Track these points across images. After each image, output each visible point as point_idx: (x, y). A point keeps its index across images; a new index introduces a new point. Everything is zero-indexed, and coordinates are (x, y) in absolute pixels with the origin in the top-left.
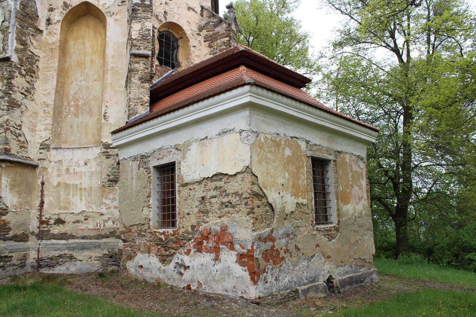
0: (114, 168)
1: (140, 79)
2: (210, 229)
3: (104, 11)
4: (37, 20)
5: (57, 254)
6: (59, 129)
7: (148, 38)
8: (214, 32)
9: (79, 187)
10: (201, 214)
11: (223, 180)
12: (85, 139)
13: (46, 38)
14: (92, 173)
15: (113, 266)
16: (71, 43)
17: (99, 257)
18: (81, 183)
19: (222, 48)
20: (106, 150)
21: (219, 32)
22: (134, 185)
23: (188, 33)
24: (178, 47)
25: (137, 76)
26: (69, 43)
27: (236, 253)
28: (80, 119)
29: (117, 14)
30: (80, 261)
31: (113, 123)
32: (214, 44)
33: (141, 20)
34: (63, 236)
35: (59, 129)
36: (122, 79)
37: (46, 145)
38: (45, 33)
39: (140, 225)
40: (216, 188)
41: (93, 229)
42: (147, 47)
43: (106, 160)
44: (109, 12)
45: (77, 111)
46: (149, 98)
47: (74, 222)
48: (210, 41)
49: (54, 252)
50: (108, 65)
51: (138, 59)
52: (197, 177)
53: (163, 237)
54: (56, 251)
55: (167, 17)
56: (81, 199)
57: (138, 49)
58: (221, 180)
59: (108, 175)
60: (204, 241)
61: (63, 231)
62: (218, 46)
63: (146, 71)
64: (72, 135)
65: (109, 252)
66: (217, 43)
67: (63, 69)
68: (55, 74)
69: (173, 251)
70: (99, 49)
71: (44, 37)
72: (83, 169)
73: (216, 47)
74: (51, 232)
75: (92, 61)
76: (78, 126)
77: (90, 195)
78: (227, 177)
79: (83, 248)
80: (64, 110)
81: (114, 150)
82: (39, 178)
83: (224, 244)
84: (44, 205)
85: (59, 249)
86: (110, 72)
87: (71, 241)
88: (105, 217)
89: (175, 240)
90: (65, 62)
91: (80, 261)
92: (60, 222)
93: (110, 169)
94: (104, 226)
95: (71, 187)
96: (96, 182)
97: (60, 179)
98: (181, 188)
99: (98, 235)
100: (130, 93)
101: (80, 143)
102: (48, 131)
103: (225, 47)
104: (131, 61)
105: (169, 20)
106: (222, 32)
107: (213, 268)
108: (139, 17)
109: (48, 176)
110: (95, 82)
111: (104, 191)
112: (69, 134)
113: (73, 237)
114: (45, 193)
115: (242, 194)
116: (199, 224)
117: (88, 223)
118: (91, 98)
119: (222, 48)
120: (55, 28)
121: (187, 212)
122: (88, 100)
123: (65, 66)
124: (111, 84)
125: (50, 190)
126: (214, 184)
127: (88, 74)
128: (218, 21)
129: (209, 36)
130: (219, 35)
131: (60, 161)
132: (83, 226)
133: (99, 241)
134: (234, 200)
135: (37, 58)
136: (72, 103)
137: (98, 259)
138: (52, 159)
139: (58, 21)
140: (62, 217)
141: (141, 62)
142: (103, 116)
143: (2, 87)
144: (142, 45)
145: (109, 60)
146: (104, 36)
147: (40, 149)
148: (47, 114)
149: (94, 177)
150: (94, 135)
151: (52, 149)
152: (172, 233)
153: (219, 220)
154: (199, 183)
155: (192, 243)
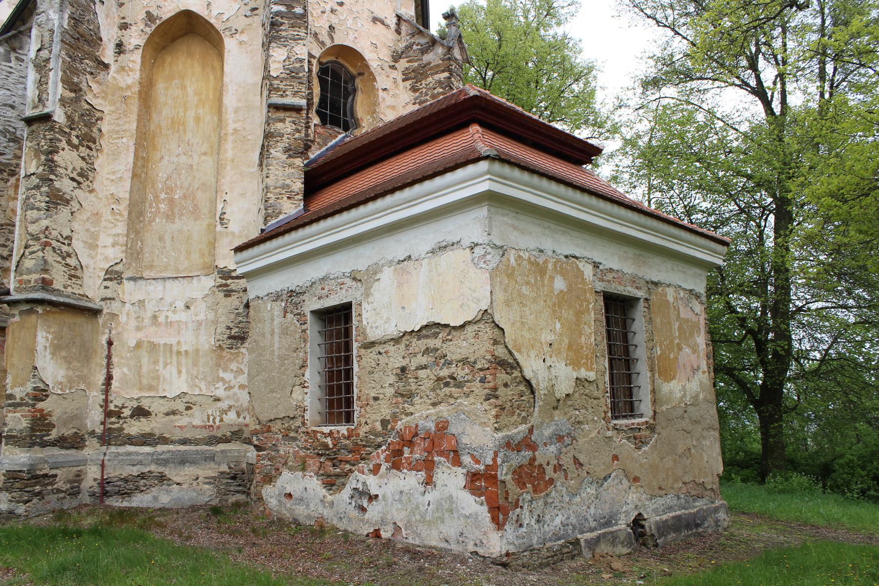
0: (238, 314)
1: (286, 150)
2: (417, 426)
3: (219, 26)
4: (99, 45)
5: (135, 471)
6: (139, 243)
7: (301, 75)
8: (421, 62)
9: (175, 349)
10: (400, 399)
11: (440, 336)
12: (186, 262)
13: (114, 78)
14: (200, 324)
15: (237, 495)
16: (160, 86)
17: (213, 478)
18: (179, 342)
19: (436, 91)
20: (224, 282)
21: (429, 63)
22: (276, 345)
23: (374, 64)
24: (355, 91)
25: (281, 146)
26: (157, 87)
27: (465, 471)
28: (178, 225)
29: (242, 32)
30: (178, 484)
31: (237, 232)
32: (421, 85)
33: (286, 43)
34: (146, 439)
35: (139, 243)
36: (252, 150)
37: (116, 272)
38: (113, 68)
39: (288, 419)
40: (427, 351)
41: (201, 427)
42: (297, 92)
43: (224, 299)
44: (229, 29)
45: (172, 211)
46: (303, 186)
47: (167, 414)
48: (413, 79)
49: (131, 467)
50: (227, 125)
51: (281, 115)
52: (392, 330)
53: (329, 441)
54: (134, 465)
55: (334, 36)
56: (179, 372)
57: (282, 96)
58: (436, 335)
59: (229, 328)
60: (405, 448)
61: (147, 430)
62: (428, 89)
63: (297, 135)
64: (162, 254)
65: (230, 468)
66: (428, 83)
67: (145, 134)
68: (132, 143)
69: (348, 467)
70: (211, 96)
71: (112, 76)
72: (183, 316)
73: (424, 90)
74: (125, 432)
75: (198, 119)
76: (173, 237)
77: (195, 365)
78: (447, 330)
79: (183, 461)
80: (147, 209)
81: (239, 281)
82: (104, 333)
83: (441, 453)
84: (113, 382)
85: (140, 463)
86: (231, 138)
87: (161, 448)
88: (223, 405)
89: (351, 446)
90: (149, 121)
91: (178, 484)
92: (140, 412)
93: (233, 316)
94: (221, 420)
95: (162, 349)
96: (207, 341)
97: (140, 335)
98: (363, 351)
99: (211, 437)
100: (267, 177)
101: (177, 270)
102: (120, 247)
103: (441, 90)
104: (269, 117)
105: (337, 42)
106: (436, 63)
107: (421, 498)
108: (283, 37)
109: (120, 329)
110: (203, 158)
111: (221, 357)
112: (157, 253)
113: (164, 440)
114: (115, 359)
115: (475, 362)
116: (395, 417)
117: (192, 416)
118: (196, 186)
119: (436, 91)
120: (132, 59)
121: (373, 395)
122: (191, 189)
123: (149, 129)
124: (233, 160)
125: (124, 355)
126: (422, 344)
127: (191, 143)
128: (427, 43)
129: (413, 71)
130: (431, 69)
131: (141, 302)
132: (183, 421)
133: (211, 448)
134: (462, 373)
135: (98, 114)
136: (163, 196)
137: (211, 480)
138: (127, 298)
139: (137, 47)
140: (145, 404)
141: (288, 120)
142: (218, 219)
143: (38, 168)
144: (288, 87)
145: (230, 116)
146: (219, 73)
147: (105, 280)
148: (118, 217)
149: (202, 331)
150: (203, 255)
151: (127, 279)
152: (346, 433)
153: (432, 411)
154: (396, 341)
155: (383, 452)
